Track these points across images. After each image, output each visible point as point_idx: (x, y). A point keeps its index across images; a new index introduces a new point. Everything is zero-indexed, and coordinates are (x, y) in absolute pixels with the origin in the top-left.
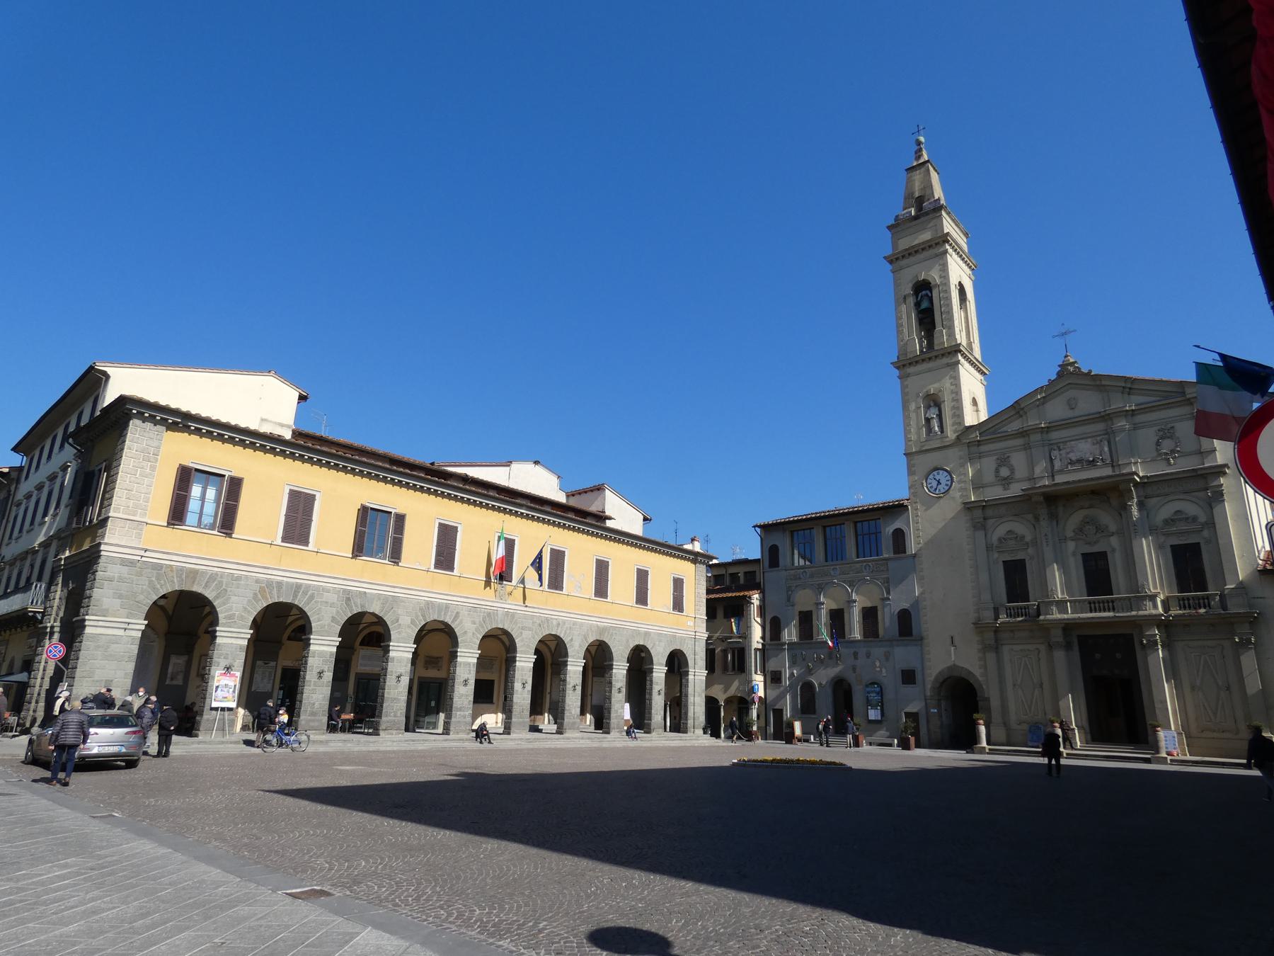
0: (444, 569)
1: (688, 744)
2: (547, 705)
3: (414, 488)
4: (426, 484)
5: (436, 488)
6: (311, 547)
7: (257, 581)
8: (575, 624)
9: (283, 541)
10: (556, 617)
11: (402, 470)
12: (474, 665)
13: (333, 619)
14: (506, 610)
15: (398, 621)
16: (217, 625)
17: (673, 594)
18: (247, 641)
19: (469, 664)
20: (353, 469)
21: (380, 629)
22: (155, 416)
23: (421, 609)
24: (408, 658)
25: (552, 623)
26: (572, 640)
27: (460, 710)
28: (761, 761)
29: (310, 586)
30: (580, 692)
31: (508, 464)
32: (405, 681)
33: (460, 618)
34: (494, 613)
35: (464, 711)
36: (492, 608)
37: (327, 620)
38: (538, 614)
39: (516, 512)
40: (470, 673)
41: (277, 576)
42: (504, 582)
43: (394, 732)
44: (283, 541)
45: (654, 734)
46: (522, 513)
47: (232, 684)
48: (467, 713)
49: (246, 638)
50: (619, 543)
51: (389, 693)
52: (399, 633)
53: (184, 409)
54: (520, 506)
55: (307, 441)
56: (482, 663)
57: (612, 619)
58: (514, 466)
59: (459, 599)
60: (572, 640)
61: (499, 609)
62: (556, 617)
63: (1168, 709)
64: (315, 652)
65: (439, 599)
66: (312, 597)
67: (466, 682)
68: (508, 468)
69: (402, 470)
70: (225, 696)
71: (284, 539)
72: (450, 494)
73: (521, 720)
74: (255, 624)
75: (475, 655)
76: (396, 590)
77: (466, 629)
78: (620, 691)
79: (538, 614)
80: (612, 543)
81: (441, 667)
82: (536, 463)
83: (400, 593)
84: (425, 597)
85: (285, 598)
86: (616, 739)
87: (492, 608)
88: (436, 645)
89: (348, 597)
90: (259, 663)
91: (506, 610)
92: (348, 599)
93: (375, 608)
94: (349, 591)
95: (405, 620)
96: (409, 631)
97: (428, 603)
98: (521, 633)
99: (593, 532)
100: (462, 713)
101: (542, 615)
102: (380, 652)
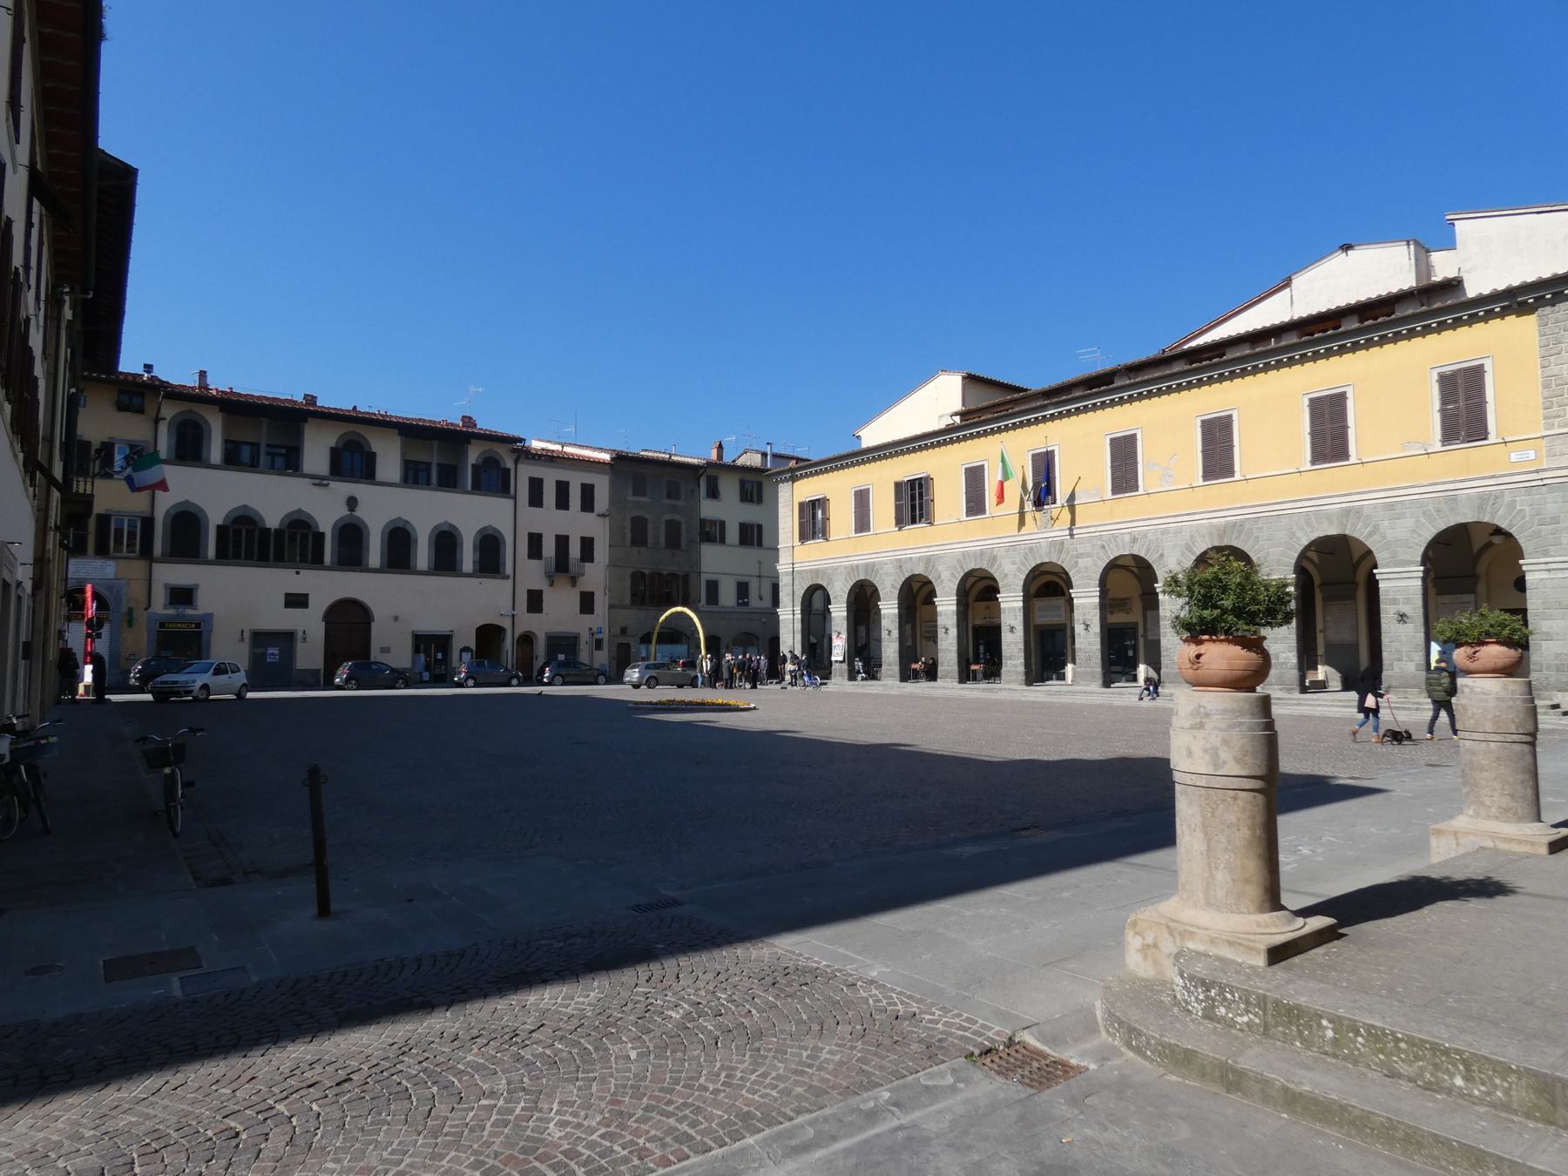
0: (976, 515)
1: (994, 696)
2: (1321, 650)
3: (1078, 411)
4: (1152, 386)
5: (1066, 408)
6: (1353, 459)
7: (845, 568)
8: (1164, 532)
9: (1204, 481)
10: (1129, 530)
11: (1064, 397)
12: (1019, 609)
13: (893, 586)
14: (1050, 539)
15: (940, 577)
16: (778, 607)
17: (1443, 411)
18: (1420, 580)
19: (1014, 608)
20: (1169, 387)
21: (985, 583)
22: (1257, 365)
23: (959, 561)
24: (953, 611)
25: (1123, 541)
26: (1162, 555)
27: (1010, 658)
28: (656, 704)
29: (874, 563)
30: (1022, 634)
31: (1287, 283)
32: (1096, 627)
33: (999, 561)
34: (1036, 547)
35: (1015, 660)
36: (1032, 542)
37: (888, 588)
38: (1098, 534)
39: (1044, 417)
40: (1016, 619)
41: (855, 561)
42: (1045, 507)
43: (949, 680)
44: (1204, 481)
45: (939, 682)
46: (1052, 415)
47: (841, 644)
48: (1018, 662)
49: (1417, 577)
50: (1007, 431)
51: (941, 645)
52: (943, 588)
53: (1501, 287)
54: (1044, 408)
55: (980, 415)
56: (1108, 603)
57: (952, 544)
58: (1299, 281)
59: (991, 542)
60: (1162, 555)
61: (1040, 541)
62: (1129, 530)
63: (6, 657)
64: (884, 615)
65: (973, 547)
66: (877, 571)
67: (1012, 629)
68: (1288, 289)
69: (1064, 397)
70: (539, 658)
71: (1114, 492)
72: (965, 435)
73: (1089, 670)
74: (1426, 559)
75: (1018, 599)
76: (896, 553)
77: (1006, 572)
78: (1402, 618)
79: (1098, 534)
80: (857, 467)
81: (1131, 609)
82: (1347, 248)
83: (936, 551)
84: (959, 549)
85: (1467, 516)
86: (1011, 686)
87: (1032, 542)
88: (1127, 587)
89: (900, 564)
90: (1148, 612)
91: (1050, 539)
92: (901, 566)
93: (919, 570)
94: (901, 559)
95: (945, 575)
96: (950, 584)
97: (963, 554)
98: (1077, 562)
99: (816, 471)
100: (1013, 662)
101: (1055, 539)
102: (1060, 601)
